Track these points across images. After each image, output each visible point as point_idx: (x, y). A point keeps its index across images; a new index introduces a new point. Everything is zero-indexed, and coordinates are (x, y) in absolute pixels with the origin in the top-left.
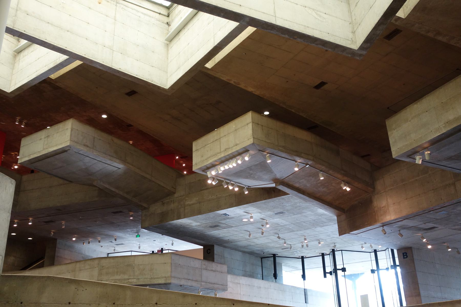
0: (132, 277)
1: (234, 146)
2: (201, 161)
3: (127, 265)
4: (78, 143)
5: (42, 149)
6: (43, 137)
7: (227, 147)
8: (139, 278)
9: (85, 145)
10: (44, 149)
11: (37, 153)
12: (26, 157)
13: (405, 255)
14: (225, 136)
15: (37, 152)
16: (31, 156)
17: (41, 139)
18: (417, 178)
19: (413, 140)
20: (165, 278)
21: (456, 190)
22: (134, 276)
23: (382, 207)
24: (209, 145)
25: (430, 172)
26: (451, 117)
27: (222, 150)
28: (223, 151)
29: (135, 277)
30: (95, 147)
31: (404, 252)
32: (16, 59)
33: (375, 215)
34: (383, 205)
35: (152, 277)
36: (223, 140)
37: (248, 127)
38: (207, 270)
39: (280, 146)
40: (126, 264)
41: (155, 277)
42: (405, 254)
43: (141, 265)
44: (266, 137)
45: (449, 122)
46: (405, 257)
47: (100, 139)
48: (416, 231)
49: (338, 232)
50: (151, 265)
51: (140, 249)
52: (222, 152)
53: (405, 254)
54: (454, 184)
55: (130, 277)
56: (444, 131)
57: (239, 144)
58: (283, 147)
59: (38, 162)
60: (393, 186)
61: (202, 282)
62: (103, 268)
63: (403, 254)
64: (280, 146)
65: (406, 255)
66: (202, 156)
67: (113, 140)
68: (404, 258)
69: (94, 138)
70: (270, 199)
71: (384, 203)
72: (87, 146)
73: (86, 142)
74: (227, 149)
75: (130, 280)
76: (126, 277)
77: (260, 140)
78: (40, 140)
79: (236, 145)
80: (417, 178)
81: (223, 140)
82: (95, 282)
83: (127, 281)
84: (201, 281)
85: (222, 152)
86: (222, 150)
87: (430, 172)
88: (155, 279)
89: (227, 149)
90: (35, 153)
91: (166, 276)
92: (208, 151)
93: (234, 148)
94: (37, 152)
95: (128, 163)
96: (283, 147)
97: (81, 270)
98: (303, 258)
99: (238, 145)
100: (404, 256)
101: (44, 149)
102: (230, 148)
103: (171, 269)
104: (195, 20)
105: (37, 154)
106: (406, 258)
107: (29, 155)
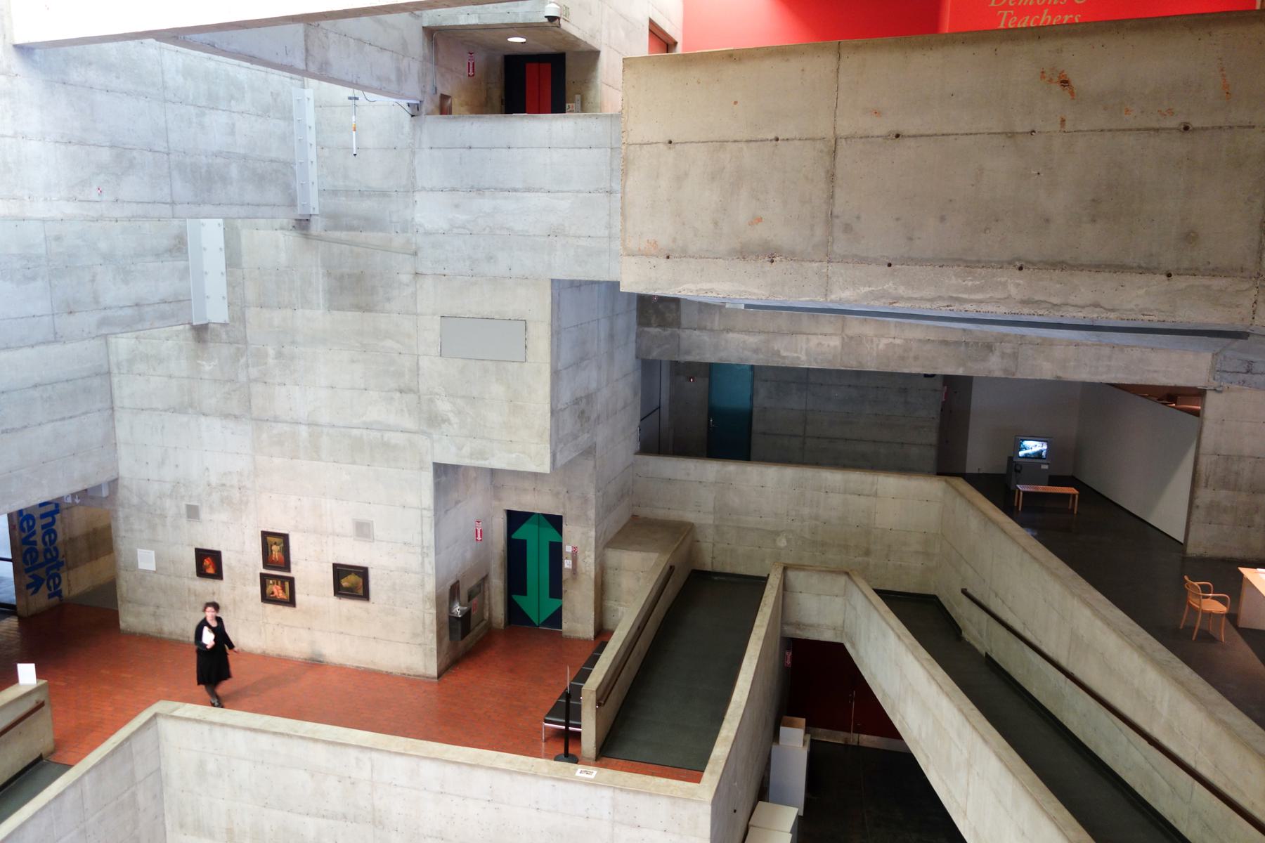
4: (684, 254)
9: (743, 253)
30: (848, 228)
32: (329, 274)
67: (1065, 83)
69: (833, 153)
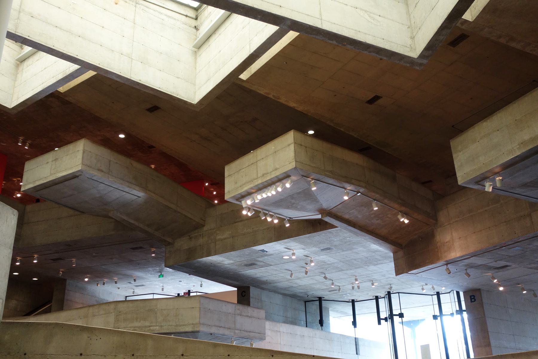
0: (154, 324)
1: (273, 171)
2: (234, 188)
3: (148, 310)
4: (91, 167)
5: (49, 174)
6: (50, 160)
7: (265, 172)
8: (162, 325)
9: (99, 170)
10: (51, 174)
11: (44, 179)
12: (30, 183)
13: (473, 299)
14: (263, 159)
15: (43, 178)
16: (37, 182)
17: (48, 163)
18: (487, 208)
19: (482, 164)
20: (192, 325)
21: (532, 222)
22: (156, 323)
23: (446, 242)
24: (243, 170)
25: (502, 201)
26: (526, 137)
27: (259, 175)
28: (261, 177)
29: (157, 324)
30: (111, 172)
31: (471, 295)
32: (18, 69)
33: (438, 251)
34: (447, 240)
35: (177, 324)
36: (260, 164)
37: (289, 148)
38: (241, 316)
39: (327, 171)
40: (147, 309)
41: (181, 324)
42: (472, 297)
43: (164, 310)
44: (310, 160)
45: (524, 143)
46: (473, 300)
47: (117, 163)
48: (486, 270)
49: (394, 271)
50: (176, 310)
51: (164, 291)
52: (259, 178)
53: (472, 297)
54: (530, 215)
55: (152, 324)
56: (518, 153)
57: (278, 169)
58: (331, 172)
59: (44, 190)
60: (459, 218)
61: (236, 330)
62: (120, 313)
63: (471, 296)
64: (327, 171)
65: (474, 298)
66: (236, 183)
67: (132, 164)
68: (472, 302)
69: (110, 162)
70: (315, 233)
71: (448, 238)
72: (102, 171)
73: (101, 166)
74: (265, 174)
75: (152, 328)
76: (147, 324)
77: (304, 164)
78: (46, 164)
79: (276, 169)
80: (487, 208)
81: (261, 164)
82: (111, 330)
83: (148, 329)
84: (235, 329)
85: (259, 178)
86: (259, 175)
87: (502, 201)
88: (180, 326)
89: (265, 174)
90: (41, 179)
91: (194, 323)
92: (242, 177)
93: (274, 172)
94: (43, 178)
95: (149, 191)
96: (331, 172)
97: (94, 316)
98: (353, 302)
99: (278, 170)
100: (471, 299)
101: (51, 174)
102: (268, 173)
103: (200, 315)
104: (228, 23)
105: (43, 180)
106: (474, 301)
107: (33, 182)
